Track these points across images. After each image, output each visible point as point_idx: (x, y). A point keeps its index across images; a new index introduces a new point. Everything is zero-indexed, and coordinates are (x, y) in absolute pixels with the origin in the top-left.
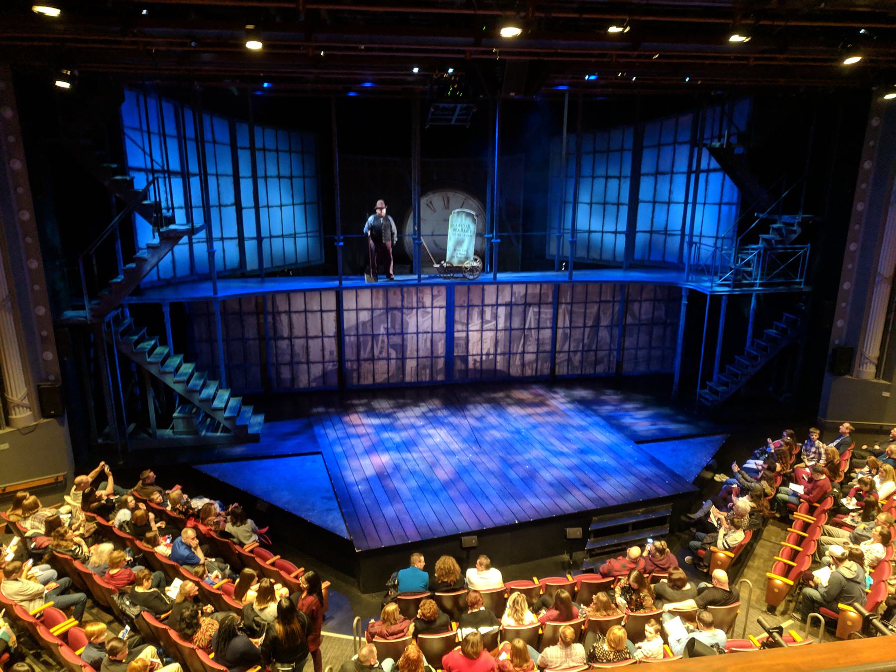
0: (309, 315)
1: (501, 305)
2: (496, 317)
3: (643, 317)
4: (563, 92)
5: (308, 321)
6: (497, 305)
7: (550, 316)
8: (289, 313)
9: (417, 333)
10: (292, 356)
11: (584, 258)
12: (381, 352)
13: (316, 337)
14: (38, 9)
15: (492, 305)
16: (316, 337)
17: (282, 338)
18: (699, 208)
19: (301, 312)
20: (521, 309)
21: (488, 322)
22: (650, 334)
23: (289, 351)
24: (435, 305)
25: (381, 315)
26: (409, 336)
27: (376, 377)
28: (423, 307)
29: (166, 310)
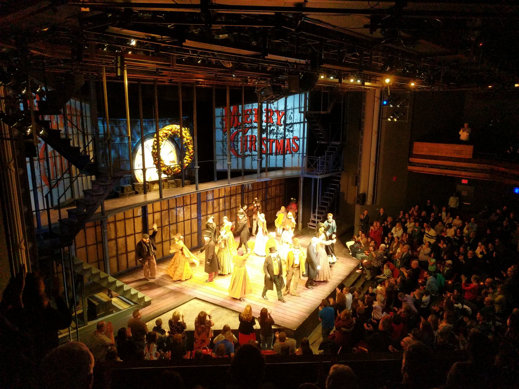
0: (127, 221)
1: (221, 198)
2: (219, 204)
3: (273, 195)
4: (117, 72)
5: (126, 225)
6: (219, 198)
7: (240, 200)
8: (115, 222)
9: (184, 221)
10: (117, 250)
11: (236, 170)
12: (166, 237)
13: (131, 235)
14: (393, 4)
15: (217, 199)
16: (131, 235)
17: (111, 240)
18: (302, 136)
19: (122, 220)
20: (229, 198)
21: (216, 208)
22: (275, 202)
23: (115, 248)
24: (192, 203)
25: (166, 213)
26: (140, 231)
27: (164, 252)
28: (187, 205)
29: (313, 180)
